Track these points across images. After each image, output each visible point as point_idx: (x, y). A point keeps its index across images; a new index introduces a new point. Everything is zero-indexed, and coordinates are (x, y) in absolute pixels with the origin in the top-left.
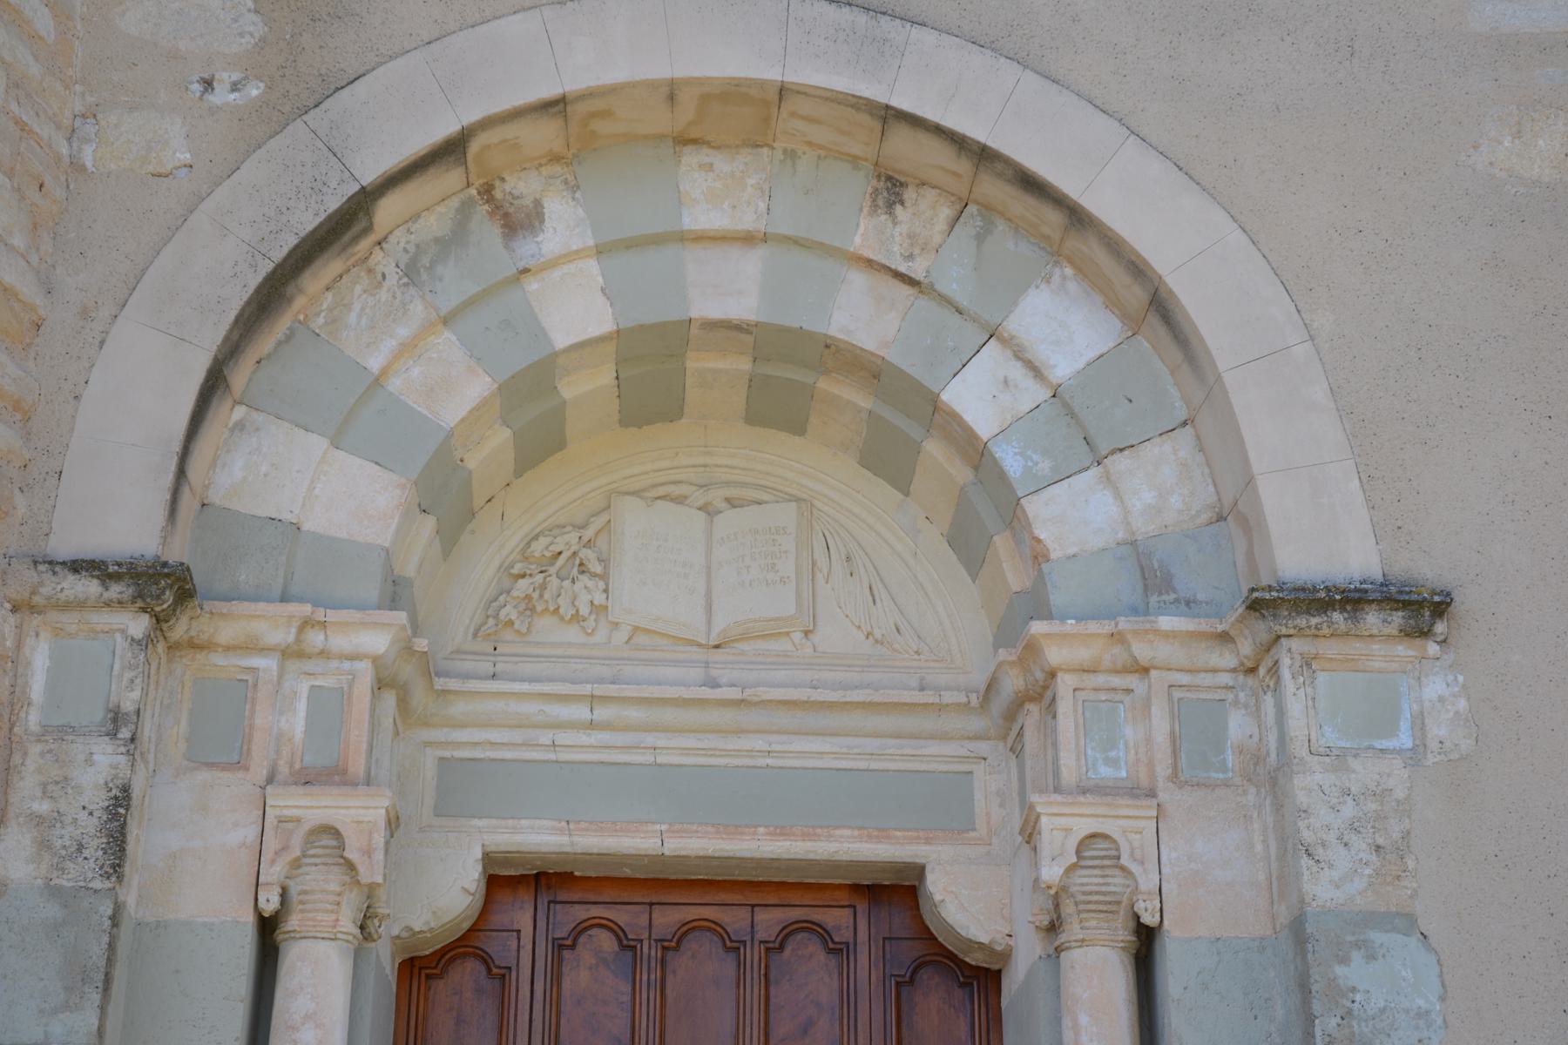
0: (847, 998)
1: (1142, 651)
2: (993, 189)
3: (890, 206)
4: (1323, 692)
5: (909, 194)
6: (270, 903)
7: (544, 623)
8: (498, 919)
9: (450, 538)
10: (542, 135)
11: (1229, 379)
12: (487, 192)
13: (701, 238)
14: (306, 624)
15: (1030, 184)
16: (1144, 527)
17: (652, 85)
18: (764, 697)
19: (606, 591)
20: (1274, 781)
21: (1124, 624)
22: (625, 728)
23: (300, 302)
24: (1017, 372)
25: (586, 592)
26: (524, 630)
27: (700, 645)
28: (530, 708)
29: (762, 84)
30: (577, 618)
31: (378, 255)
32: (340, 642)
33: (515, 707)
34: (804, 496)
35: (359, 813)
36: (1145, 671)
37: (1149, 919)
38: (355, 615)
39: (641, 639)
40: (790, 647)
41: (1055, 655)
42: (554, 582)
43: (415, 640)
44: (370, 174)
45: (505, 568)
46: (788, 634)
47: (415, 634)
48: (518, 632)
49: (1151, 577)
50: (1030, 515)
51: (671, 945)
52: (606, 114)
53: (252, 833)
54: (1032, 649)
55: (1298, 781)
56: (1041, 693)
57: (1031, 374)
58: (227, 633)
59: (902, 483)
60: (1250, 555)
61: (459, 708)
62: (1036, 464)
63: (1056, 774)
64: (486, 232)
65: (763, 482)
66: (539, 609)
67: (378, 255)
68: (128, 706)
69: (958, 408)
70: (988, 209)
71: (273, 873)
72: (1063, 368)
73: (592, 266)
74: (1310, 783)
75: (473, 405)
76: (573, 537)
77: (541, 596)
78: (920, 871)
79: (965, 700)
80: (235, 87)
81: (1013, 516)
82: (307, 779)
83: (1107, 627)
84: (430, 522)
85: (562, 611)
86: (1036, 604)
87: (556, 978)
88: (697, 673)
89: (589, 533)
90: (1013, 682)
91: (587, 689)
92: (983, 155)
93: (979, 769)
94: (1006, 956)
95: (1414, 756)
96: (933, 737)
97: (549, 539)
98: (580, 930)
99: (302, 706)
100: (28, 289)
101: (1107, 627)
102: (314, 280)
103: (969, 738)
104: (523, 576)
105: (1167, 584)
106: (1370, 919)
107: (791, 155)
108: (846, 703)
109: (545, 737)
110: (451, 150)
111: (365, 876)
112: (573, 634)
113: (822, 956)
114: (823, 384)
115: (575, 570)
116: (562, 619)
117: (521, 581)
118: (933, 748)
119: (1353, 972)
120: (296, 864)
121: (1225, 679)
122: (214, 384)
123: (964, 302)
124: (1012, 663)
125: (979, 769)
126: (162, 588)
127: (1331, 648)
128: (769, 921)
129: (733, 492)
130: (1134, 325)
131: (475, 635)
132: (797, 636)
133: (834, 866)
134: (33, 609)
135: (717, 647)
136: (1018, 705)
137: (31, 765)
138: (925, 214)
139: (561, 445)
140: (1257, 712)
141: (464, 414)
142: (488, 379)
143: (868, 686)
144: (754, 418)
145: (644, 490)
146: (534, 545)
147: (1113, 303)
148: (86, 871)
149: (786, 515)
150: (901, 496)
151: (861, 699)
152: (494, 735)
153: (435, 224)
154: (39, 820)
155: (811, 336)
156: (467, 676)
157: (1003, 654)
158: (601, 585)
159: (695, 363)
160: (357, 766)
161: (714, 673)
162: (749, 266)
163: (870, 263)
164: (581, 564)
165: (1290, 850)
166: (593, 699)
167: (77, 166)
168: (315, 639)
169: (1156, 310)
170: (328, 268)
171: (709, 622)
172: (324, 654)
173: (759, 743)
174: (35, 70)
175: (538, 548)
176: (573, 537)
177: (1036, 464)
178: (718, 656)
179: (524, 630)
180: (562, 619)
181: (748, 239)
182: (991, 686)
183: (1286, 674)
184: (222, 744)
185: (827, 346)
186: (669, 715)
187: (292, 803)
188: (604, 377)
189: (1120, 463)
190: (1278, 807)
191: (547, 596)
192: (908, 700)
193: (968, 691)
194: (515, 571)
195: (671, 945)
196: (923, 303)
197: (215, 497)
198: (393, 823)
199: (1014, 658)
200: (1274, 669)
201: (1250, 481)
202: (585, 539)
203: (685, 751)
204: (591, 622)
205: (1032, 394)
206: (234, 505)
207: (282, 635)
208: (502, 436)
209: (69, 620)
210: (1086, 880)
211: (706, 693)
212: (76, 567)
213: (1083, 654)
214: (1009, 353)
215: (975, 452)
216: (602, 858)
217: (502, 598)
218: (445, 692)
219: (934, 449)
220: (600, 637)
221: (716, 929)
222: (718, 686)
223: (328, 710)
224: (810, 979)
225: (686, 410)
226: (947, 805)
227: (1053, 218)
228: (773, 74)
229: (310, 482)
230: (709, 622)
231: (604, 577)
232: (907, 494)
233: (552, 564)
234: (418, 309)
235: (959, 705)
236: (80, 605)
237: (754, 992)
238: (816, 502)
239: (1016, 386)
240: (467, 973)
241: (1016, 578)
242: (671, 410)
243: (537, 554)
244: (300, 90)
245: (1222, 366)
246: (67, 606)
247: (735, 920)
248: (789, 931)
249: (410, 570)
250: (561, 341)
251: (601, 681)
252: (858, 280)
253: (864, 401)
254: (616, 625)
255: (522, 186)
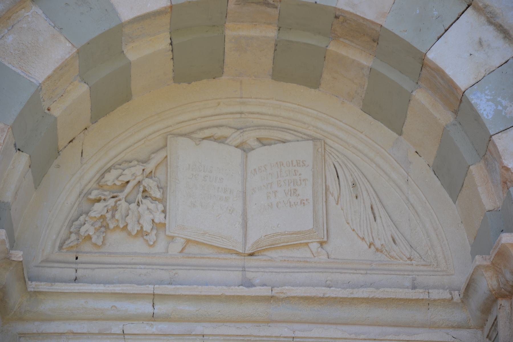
9: (39, 171)
18: (289, 294)
19: (164, 212)
22: (181, 319)
24: (490, 34)
25: (148, 213)
26: (100, 243)
27: (238, 253)
28: (105, 304)
30: (141, 233)
33: (93, 304)
34: (319, 136)
39: (192, 249)
40: (309, 255)
42: (123, 205)
43: (12, 252)
45: (84, 195)
46: (307, 244)
47: (12, 247)
48: (95, 245)
50: (500, 149)
57: (502, 36)
59: (396, 124)
62: (505, 108)
65: (287, 126)
66: (111, 226)
69: (442, 64)
75: (57, 65)
76: (138, 170)
77: (113, 216)
79: (449, 296)
84: (24, 159)
85: (129, 228)
88: (236, 276)
89: (150, 167)
91: (149, 289)
96: (423, 326)
97: (120, 171)
103: (453, 327)
104: (99, 201)
108: (353, 299)
112: (138, 246)
114: (333, 47)
115: (140, 196)
116: (130, 234)
117: (97, 205)
124: (487, 267)
129: (263, 134)
131: (61, 247)
132: (314, 246)
135: (251, 255)
139: (127, 97)
141: (49, 72)
142: (68, 45)
143: (371, 285)
144: (279, 74)
145: (193, 132)
146: (108, 176)
149: (305, 151)
150: (395, 135)
151: (365, 295)
155: (324, 9)
156: (54, 280)
157: (479, 260)
158: (161, 207)
161: (249, 275)
164: (144, 191)
166: (154, 297)
171: (245, 235)
175: (110, 178)
176: (138, 170)
177: (505, 108)
179: (100, 243)
180: (130, 234)
185: (337, 17)
186: (214, 309)
188: (162, 43)
191: (118, 216)
192: (403, 296)
193: (451, 290)
194: (92, 197)
199: (488, 263)
202: (148, 171)
204: (152, 237)
214: (483, 19)
215: (456, 100)
217: (82, 218)
218: (37, 293)
219: (422, 97)
220: (160, 247)
222: (253, 285)
225: (226, 69)
230: (245, 235)
231: (163, 201)
232: (400, 134)
233: (122, 191)
235: (444, 300)
238: (328, 141)
239: (489, 45)
242: (214, 69)
243: (109, 183)
250: (126, 14)
251: (161, 282)
254: (172, 238)
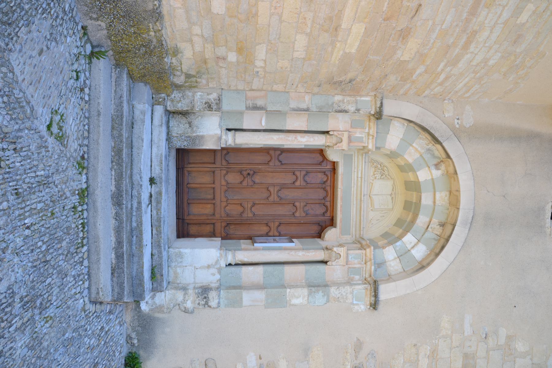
0: (317, 215)
1: (368, 263)
2: (442, 241)
3: (440, 225)
4: (362, 291)
5: (441, 228)
6: (331, 133)
7: (373, 169)
8: (328, 163)
10: (451, 170)
11: (411, 278)
12: (442, 161)
13: (435, 195)
14: (373, 136)
15: (443, 248)
16: (388, 264)
17: (459, 188)
20: (348, 283)
21: (373, 261)
23: (424, 133)
24: (413, 244)
25: (378, 176)
29: (460, 205)
30: (374, 174)
31: (431, 145)
32: (370, 141)
33: (360, 166)
35: (344, 145)
36: (365, 264)
37: (328, 263)
38: (374, 143)
39: (371, 184)
41: (368, 250)
44: (444, 144)
45: (382, 163)
49: (380, 265)
51: (324, 189)
52: (455, 180)
53: (341, 130)
54: (369, 247)
55: (348, 287)
56: (362, 248)
58: (372, 124)
59: (396, 225)
60: (383, 280)
61: (360, 157)
63: (350, 250)
64: (435, 161)
67: (431, 145)
68: (360, 112)
70: (439, 240)
71: (335, 133)
72: (413, 252)
73: (430, 178)
74: (348, 288)
78: (335, 227)
80: (458, 123)
81: (390, 243)
82: (349, 137)
83: (372, 258)
86: (376, 247)
87: (320, 172)
88: (366, 193)
90: (364, 243)
92: (447, 240)
93: (351, 236)
94: (323, 240)
95: (352, 304)
98: (327, 175)
99: (360, 136)
100: (424, 94)
101: (372, 258)
102: (427, 135)
105: (379, 267)
106: (328, 296)
107: (448, 209)
109: (356, 170)
110: (448, 156)
111: (335, 147)
112: (372, 174)
113: (323, 211)
114: (411, 213)
118: (354, 229)
119: (321, 293)
120: (337, 136)
121: (364, 276)
122: (410, 121)
123: (424, 236)
125: (351, 236)
126: (379, 115)
127: (368, 292)
128: (328, 204)
130: (420, 263)
133: (336, 214)
134: (375, 97)
136: (360, 243)
137: (352, 99)
138: (438, 230)
140: (359, 280)
147: (423, 260)
148: (336, 107)
152: (356, 163)
153: (437, 153)
154: (343, 100)
155: (419, 212)
156: (365, 158)
157: (368, 241)
159: (415, 194)
160: (351, 144)
162: (430, 203)
163: (430, 222)
165: (338, 285)
166: (361, 178)
167: (444, 100)
168: (371, 137)
169: (422, 267)
170: (429, 138)
172: (368, 139)
173: (355, 203)
174: (459, 94)
175: (385, 168)
176: (387, 173)
178: (368, 196)
181: (434, 202)
182: (363, 239)
183: (365, 286)
184: (354, 124)
186: (359, 189)
187: (346, 135)
188: (412, 179)
189: (398, 260)
190: (345, 283)
195: (324, 189)
196: (424, 230)
197: (393, 122)
198: (343, 150)
200: (365, 284)
201: (395, 281)
203: (354, 192)
205: (409, 247)
206: (391, 126)
207: (371, 132)
208: (403, 163)
209: (373, 102)
210: (334, 254)
211: (363, 195)
212: (382, 103)
213: (368, 254)
215: (400, 238)
216: (337, 177)
219: (401, 231)
220: (371, 178)
221: (327, 196)
223: (360, 140)
224: (320, 210)
226: (345, 231)
227: (437, 250)
228: (461, 207)
229: (395, 137)
234: (423, 151)
236: (376, 104)
237: (317, 202)
240: (321, 159)
241: (380, 243)
242: (407, 189)
244: (458, 133)
245: (413, 277)
246: (375, 102)
247: (328, 199)
248: (326, 207)
249: (381, 150)
250: (418, 173)
252: (428, 220)
253: (408, 220)
255: (443, 167)
